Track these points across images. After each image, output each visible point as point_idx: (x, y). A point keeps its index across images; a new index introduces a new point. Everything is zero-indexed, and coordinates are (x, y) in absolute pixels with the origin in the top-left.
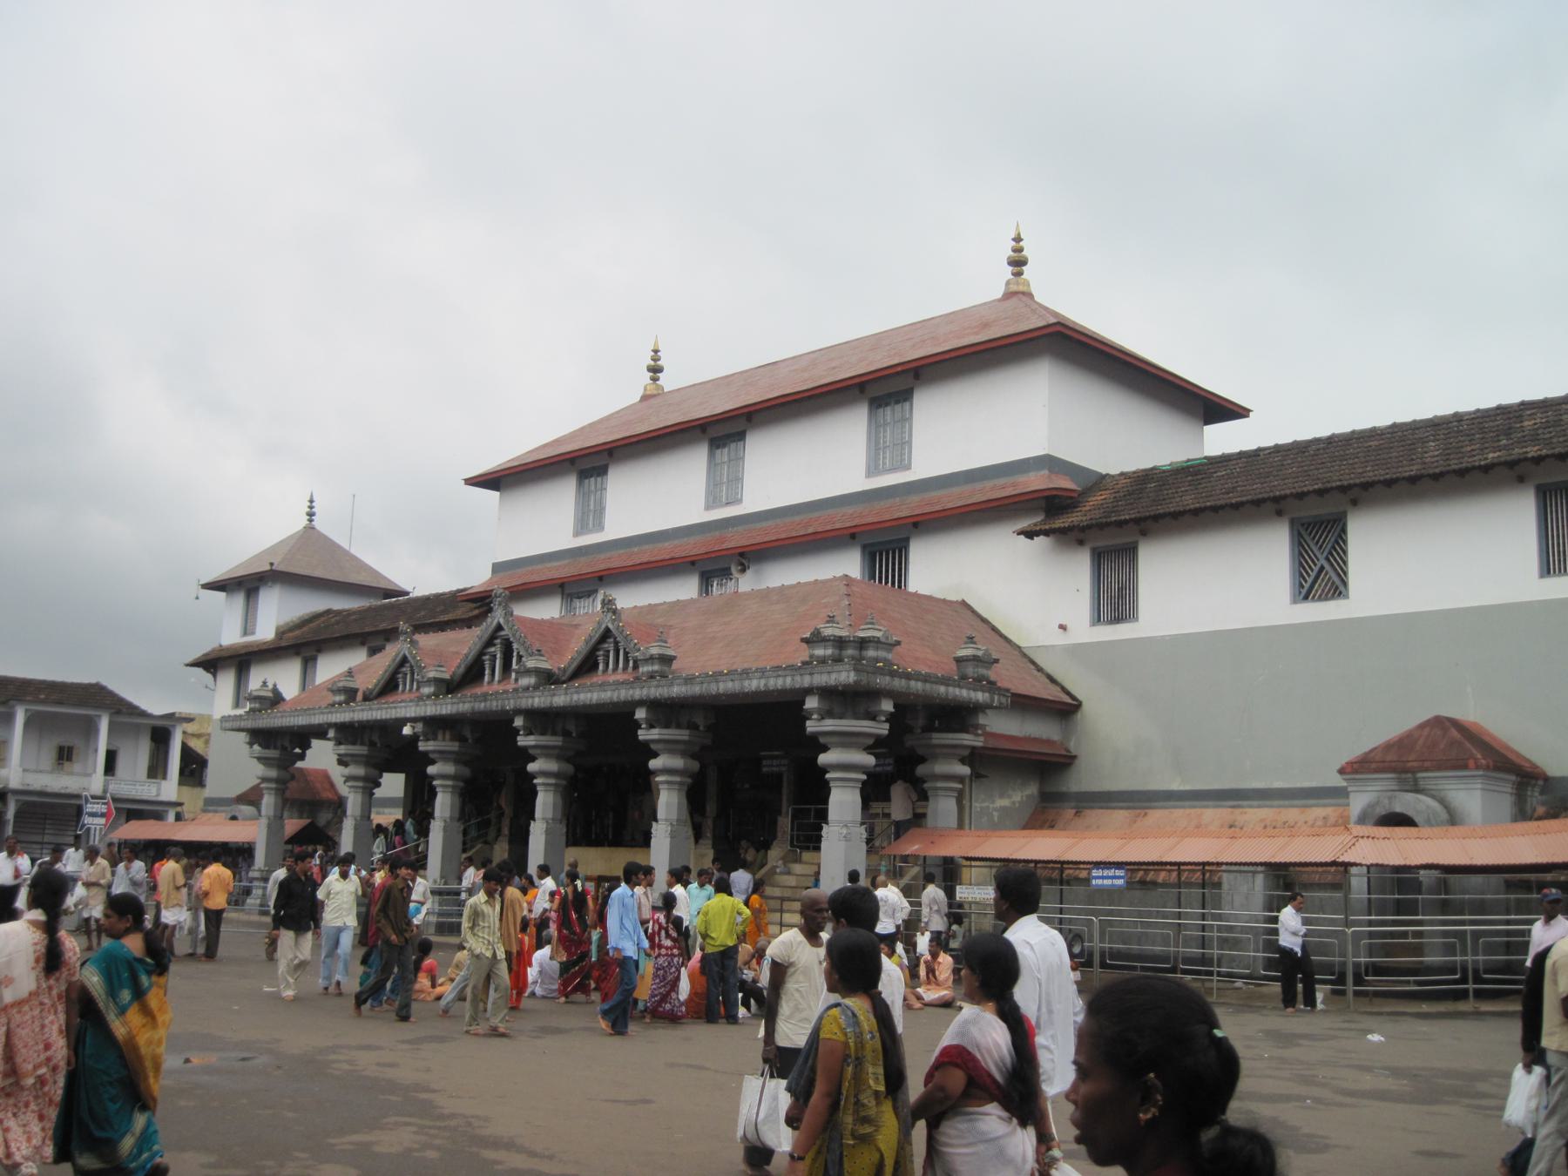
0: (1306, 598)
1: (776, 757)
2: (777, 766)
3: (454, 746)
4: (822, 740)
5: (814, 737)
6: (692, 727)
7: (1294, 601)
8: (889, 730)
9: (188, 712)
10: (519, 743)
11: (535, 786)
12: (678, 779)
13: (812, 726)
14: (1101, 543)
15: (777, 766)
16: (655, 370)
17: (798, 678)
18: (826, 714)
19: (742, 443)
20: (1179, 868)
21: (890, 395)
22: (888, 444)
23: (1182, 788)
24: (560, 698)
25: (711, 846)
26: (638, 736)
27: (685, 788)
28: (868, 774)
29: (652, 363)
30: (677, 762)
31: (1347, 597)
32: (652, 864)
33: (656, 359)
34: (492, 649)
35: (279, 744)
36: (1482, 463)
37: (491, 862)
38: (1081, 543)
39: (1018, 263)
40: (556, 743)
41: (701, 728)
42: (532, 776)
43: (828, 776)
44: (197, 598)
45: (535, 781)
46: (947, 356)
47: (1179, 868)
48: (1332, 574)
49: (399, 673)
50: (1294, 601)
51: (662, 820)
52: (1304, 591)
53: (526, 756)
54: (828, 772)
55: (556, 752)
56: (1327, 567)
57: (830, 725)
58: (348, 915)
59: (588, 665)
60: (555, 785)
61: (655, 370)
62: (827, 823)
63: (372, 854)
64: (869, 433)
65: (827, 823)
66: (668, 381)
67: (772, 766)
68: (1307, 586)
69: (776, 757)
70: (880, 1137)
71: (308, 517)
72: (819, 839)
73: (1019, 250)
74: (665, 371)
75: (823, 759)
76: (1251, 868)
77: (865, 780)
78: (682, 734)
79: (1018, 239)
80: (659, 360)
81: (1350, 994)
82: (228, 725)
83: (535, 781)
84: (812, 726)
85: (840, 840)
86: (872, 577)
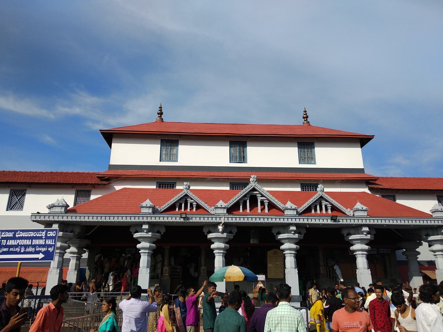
2: (386, 251)
8: (374, 238)
11: (140, 254)
12: (222, 251)
13: (34, 232)
15: (386, 251)
21: (238, 142)
27: (151, 255)
30: (222, 245)
31: (22, 210)
32: (67, 280)
36: (392, 188)
37: (239, 290)
43: (214, 252)
53: (211, 242)
62: (286, 269)
63: (278, 294)
67: (384, 251)
77: (297, 254)
82: (38, 219)
86: (303, 190)
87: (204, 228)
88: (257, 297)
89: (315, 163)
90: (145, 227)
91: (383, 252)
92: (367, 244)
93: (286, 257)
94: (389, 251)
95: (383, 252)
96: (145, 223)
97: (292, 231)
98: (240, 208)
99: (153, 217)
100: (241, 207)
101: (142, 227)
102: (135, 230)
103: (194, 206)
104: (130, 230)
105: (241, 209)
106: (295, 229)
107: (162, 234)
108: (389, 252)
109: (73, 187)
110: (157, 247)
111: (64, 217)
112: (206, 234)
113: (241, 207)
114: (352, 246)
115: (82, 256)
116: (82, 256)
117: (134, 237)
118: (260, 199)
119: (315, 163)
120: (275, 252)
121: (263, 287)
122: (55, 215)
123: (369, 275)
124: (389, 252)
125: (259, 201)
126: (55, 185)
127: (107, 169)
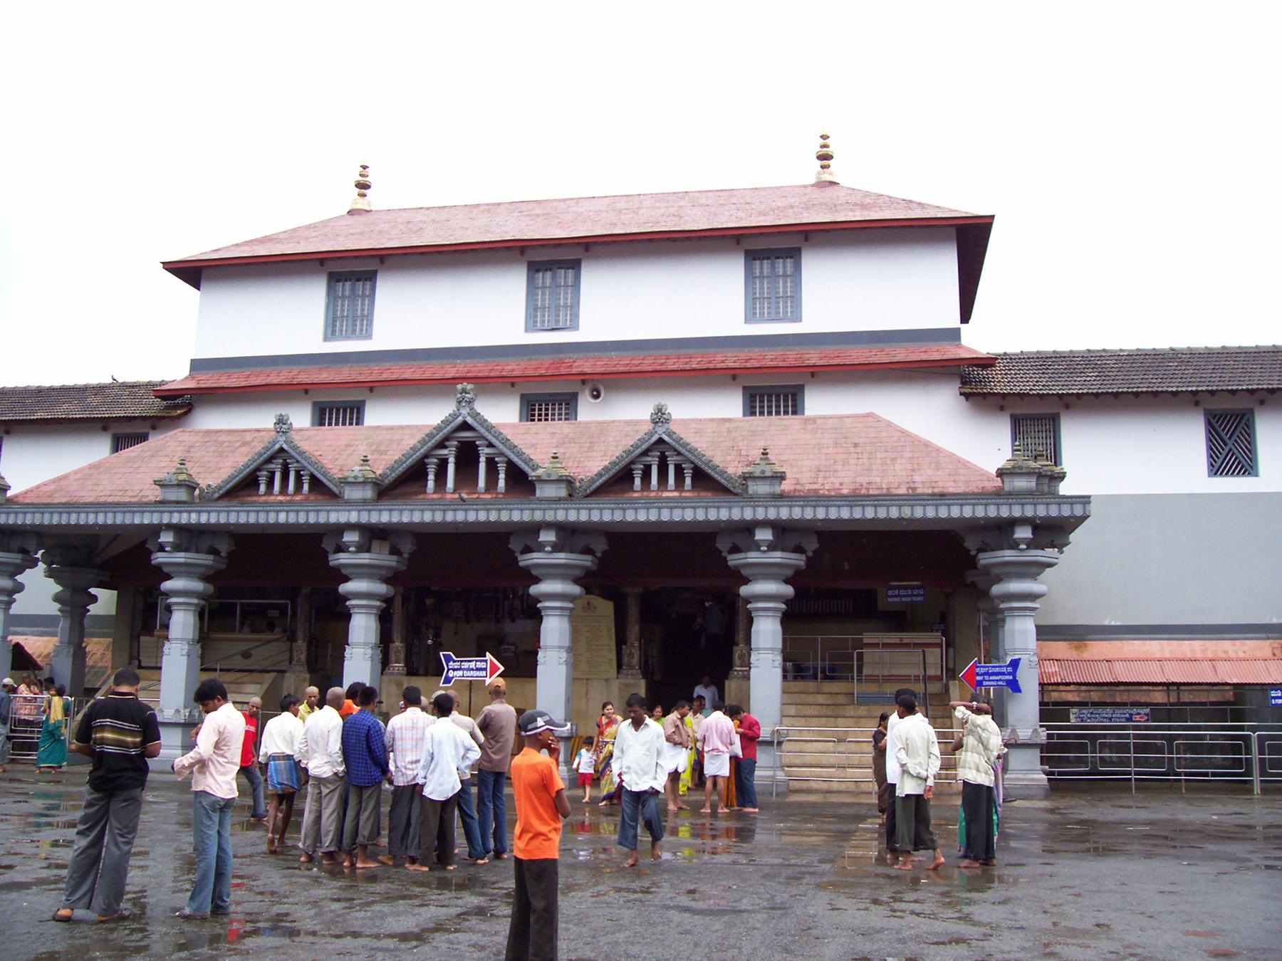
1: (913, 588)
3: (391, 561)
4: (344, 571)
5: (159, 567)
6: (214, 551)
7: (1209, 476)
12: (195, 601)
14: (1019, 411)
17: (38, 516)
18: (177, 548)
19: (368, 285)
20: (1178, 689)
22: (758, 296)
23: (1113, 623)
24: (385, 516)
25: (641, 676)
26: (727, 561)
28: (786, 603)
29: (360, 178)
34: (445, 452)
38: (1002, 408)
40: (15, 561)
41: (223, 554)
46: (445, 249)
47: (1178, 689)
51: (358, 644)
52: (1214, 471)
55: (569, 571)
57: (180, 557)
58: (249, 769)
59: (244, 486)
64: (328, 305)
65: (348, 645)
66: (375, 200)
69: (913, 588)
72: (534, 664)
74: (372, 186)
75: (345, 588)
76: (1206, 687)
78: (205, 559)
81: (1257, 788)
84: (159, 558)
85: (560, 664)
87: (511, 537)
88: (716, 708)
89: (797, 317)
90: (548, 537)
91: (909, 599)
92: (787, 581)
93: (353, 616)
94: (918, 595)
95: (909, 599)
96: (1023, 521)
97: (1023, 540)
98: (498, 479)
99: (242, 511)
100: (431, 477)
101: (539, 537)
102: (732, 545)
103: (306, 480)
104: (509, 546)
105: (431, 484)
106: (1030, 536)
107: (599, 555)
108: (919, 599)
109: (105, 429)
110: (220, 592)
111: (310, 513)
112: (973, 553)
113: (431, 477)
114: (537, 583)
115: (89, 611)
116: (89, 611)
117: (521, 564)
118: (484, 452)
119: (797, 317)
120: (589, 603)
121: (503, 688)
122: (854, 503)
123: (561, 666)
124: (919, 599)
125: (482, 459)
126: (89, 422)
127: (185, 371)
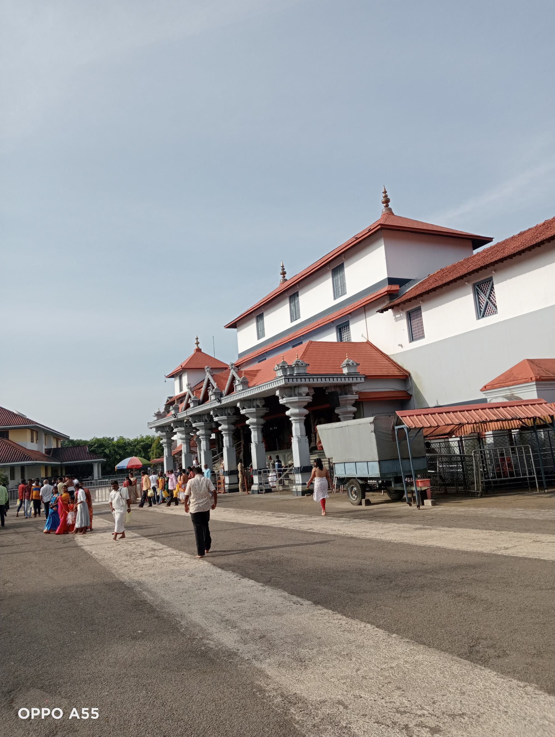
0: (483, 316)
9: (79, 439)
10: (280, 403)
11: (290, 421)
13: (282, 401)
16: (284, 273)
33: (283, 269)
35: (296, 392)
39: (387, 201)
42: (288, 417)
44: (165, 382)
45: (290, 419)
48: (491, 304)
49: (208, 390)
50: (478, 318)
54: (291, 417)
56: (489, 302)
60: (299, 420)
61: (284, 273)
66: (287, 277)
68: (482, 310)
70: (422, 647)
71: (282, 276)
73: (386, 196)
79: (385, 192)
80: (284, 270)
83: (290, 419)
